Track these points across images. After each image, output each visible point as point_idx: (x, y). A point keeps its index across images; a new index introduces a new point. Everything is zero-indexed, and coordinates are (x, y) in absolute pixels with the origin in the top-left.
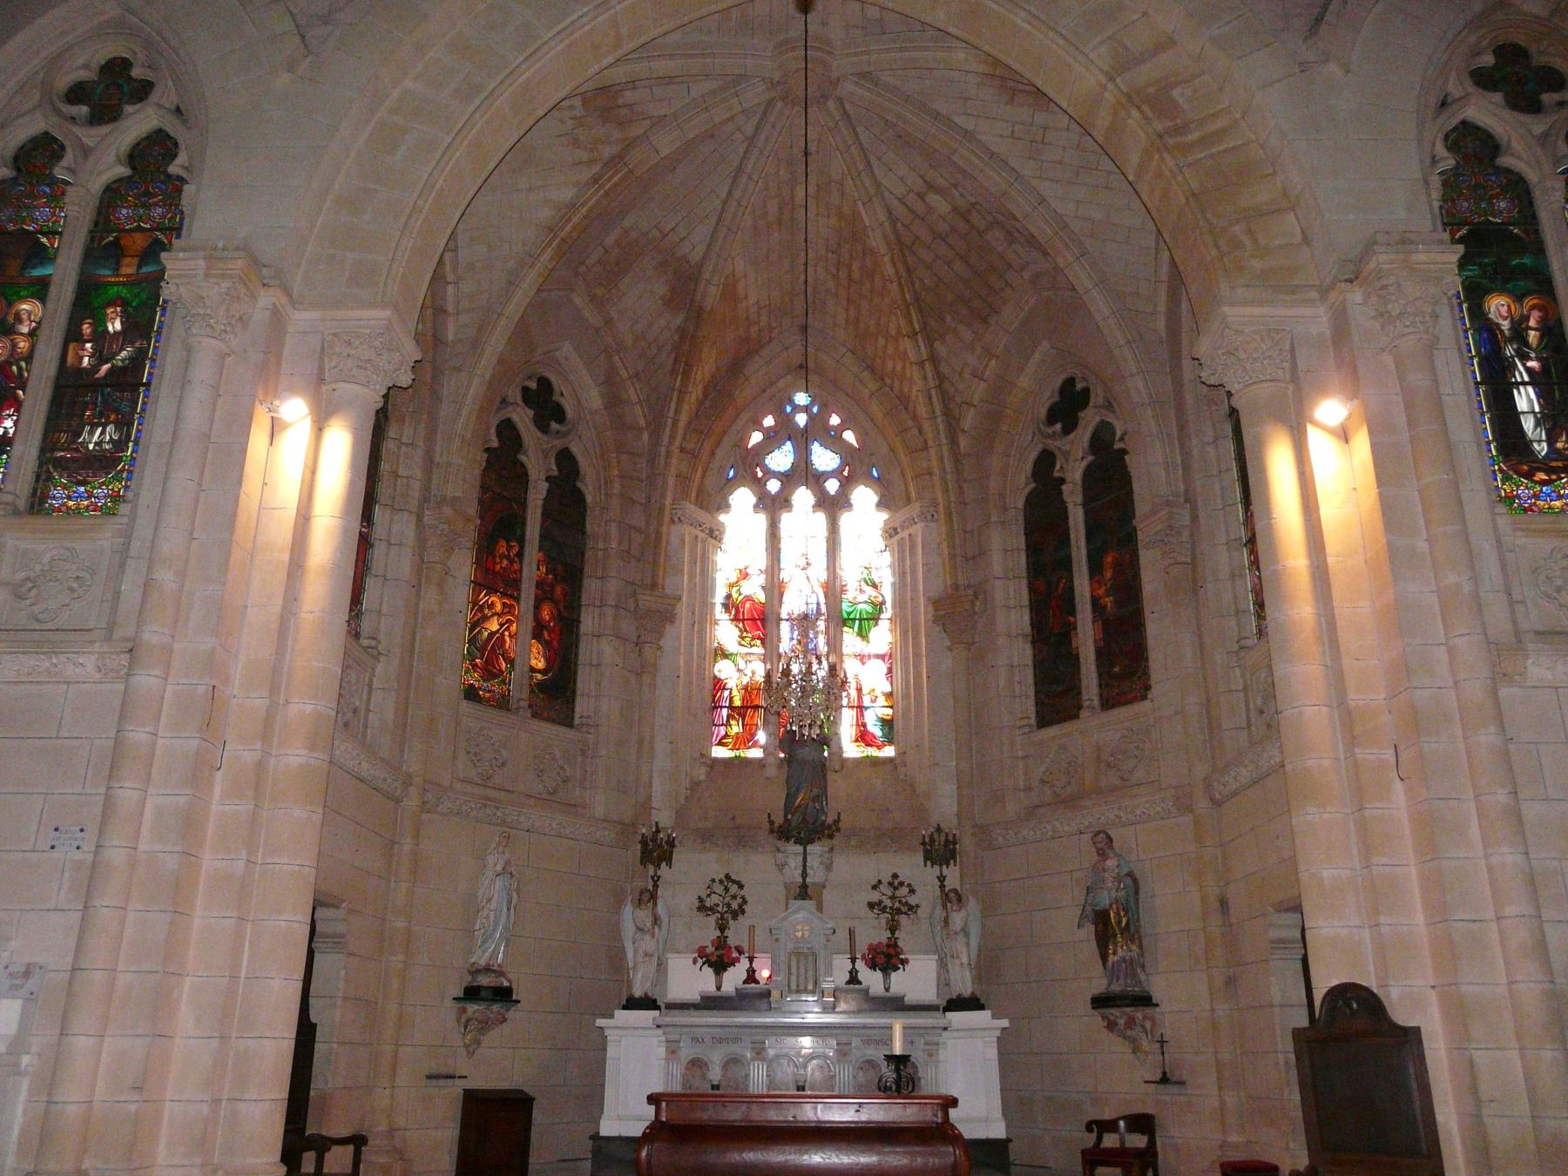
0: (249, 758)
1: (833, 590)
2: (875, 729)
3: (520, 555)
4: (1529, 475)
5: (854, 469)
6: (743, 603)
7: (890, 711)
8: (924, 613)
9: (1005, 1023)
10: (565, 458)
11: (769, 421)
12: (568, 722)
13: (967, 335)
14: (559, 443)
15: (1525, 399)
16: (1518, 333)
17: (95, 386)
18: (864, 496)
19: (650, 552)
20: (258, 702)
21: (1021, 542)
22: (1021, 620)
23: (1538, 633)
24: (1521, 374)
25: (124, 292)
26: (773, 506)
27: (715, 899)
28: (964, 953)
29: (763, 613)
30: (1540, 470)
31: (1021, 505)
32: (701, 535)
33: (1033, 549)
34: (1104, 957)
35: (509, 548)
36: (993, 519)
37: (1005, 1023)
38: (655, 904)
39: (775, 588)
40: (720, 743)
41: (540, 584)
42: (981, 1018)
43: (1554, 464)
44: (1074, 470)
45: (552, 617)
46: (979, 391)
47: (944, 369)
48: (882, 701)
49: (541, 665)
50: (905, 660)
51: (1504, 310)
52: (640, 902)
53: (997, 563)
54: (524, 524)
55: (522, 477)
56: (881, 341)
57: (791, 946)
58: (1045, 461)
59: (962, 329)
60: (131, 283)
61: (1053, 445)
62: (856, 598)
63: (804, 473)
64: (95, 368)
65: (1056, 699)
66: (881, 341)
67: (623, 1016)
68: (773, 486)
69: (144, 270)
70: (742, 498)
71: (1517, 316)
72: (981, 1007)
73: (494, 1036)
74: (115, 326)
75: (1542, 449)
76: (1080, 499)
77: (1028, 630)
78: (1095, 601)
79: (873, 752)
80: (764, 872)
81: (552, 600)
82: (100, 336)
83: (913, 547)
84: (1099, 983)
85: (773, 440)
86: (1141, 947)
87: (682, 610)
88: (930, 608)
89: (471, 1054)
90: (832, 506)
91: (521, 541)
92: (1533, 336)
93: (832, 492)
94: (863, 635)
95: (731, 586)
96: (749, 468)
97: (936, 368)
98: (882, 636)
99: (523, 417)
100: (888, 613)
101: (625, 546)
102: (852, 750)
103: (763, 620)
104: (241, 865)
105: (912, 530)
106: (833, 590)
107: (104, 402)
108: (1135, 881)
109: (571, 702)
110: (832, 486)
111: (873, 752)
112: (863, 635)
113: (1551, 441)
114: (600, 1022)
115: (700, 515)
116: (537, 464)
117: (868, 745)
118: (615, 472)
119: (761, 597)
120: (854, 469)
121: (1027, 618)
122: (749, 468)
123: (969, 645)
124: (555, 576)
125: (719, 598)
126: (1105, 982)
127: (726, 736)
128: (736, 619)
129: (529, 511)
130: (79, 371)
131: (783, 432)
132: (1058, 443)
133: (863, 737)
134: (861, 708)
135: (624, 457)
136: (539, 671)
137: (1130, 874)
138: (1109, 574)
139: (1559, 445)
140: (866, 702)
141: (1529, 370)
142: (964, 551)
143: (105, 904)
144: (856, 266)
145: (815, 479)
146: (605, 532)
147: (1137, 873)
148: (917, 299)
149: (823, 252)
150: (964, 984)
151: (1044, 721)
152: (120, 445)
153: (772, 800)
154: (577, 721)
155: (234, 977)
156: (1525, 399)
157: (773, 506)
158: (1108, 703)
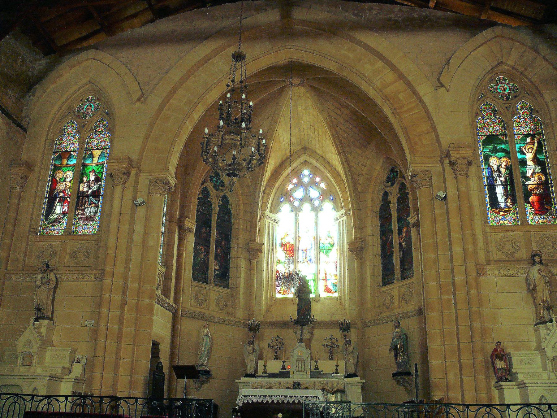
0: (134, 301)
1: (317, 240)
2: (331, 287)
3: (210, 232)
4: (498, 213)
5: (325, 195)
6: (286, 245)
7: (336, 281)
8: (346, 247)
9: (363, 381)
10: (224, 198)
11: (295, 181)
12: (226, 286)
13: (359, 151)
14: (222, 194)
15: (500, 190)
16: (499, 170)
17: (88, 196)
18: (328, 205)
19: (252, 227)
20: (136, 285)
21: (379, 223)
22: (378, 249)
23: (495, 261)
24: (498, 182)
25: (95, 168)
26: (296, 210)
27: (274, 344)
28: (352, 360)
29: (293, 248)
30: (502, 211)
31: (378, 210)
32: (272, 222)
33: (382, 225)
34: (396, 359)
35: (206, 230)
36: (369, 215)
37: (363, 381)
38: (253, 345)
39: (297, 239)
40: (279, 293)
41: (217, 241)
42: (357, 379)
43: (506, 209)
44: (393, 199)
45: (221, 252)
46: (365, 170)
47: (351, 164)
48: (334, 277)
49: (217, 268)
50: (340, 264)
51: (495, 162)
52: (250, 344)
53: (369, 230)
54: (211, 222)
55: (210, 204)
56: (330, 154)
57: (296, 357)
58: (386, 194)
59: (358, 150)
60: (97, 164)
61: (388, 190)
62: (324, 241)
63: (306, 199)
64: (88, 191)
65: (387, 276)
66: (330, 154)
67: (244, 379)
68: (296, 204)
69: (100, 161)
70: (285, 207)
71: (498, 164)
72: (357, 377)
73: (205, 386)
74: (92, 178)
75: (503, 205)
76: (396, 209)
77: (380, 253)
78: (400, 244)
79: (330, 295)
80: (291, 335)
81: (220, 246)
82: (88, 182)
83: (343, 224)
84: (395, 369)
85: (296, 186)
86: (408, 357)
87: (265, 249)
88: (348, 246)
89: (198, 391)
90: (316, 209)
91: (210, 227)
92: (503, 171)
93: (317, 205)
94: (327, 255)
95: (282, 239)
96: (287, 196)
97: (348, 164)
98: (334, 255)
99: (210, 185)
100: (336, 247)
101: (245, 227)
102: (323, 295)
103: (293, 250)
104: (133, 330)
105: (342, 219)
106: (317, 240)
107: (91, 200)
108: (407, 337)
109: (227, 280)
110: (317, 203)
111: (330, 295)
112: (327, 255)
113: (506, 203)
114: (237, 381)
115: (271, 215)
116: (216, 204)
117: (329, 292)
118: (241, 202)
119: (292, 242)
120: (325, 195)
121: (380, 248)
122: (287, 196)
123: (361, 259)
124: (222, 239)
125: (278, 242)
126: (396, 369)
127: (281, 290)
128: (284, 250)
129: (213, 217)
130: (83, 192)
131: (300, 184)
132: (389, 189)
133: (327, 290)
134: (326, 280)
135: (244, 197)
136: (217, 270)
137: (405, 334)
138: (404, 235)
139: (508, 204)
140: (328, 277)
141: (501, 181)
142: (359, 225)
143: (101, 340)
144: (320, 130)
145: (311, 200)
146: (239, 225)
147: (408, 334)
148: (340, 142)
149: (309, 126)
150: (352, 370)
151: (385, 284)
152: (95, 214)
153: (292, 312)
154: (230, 287)
155: (133, 360)
156: (500, 190)
157: (296, 210)
158: (403, 278)
